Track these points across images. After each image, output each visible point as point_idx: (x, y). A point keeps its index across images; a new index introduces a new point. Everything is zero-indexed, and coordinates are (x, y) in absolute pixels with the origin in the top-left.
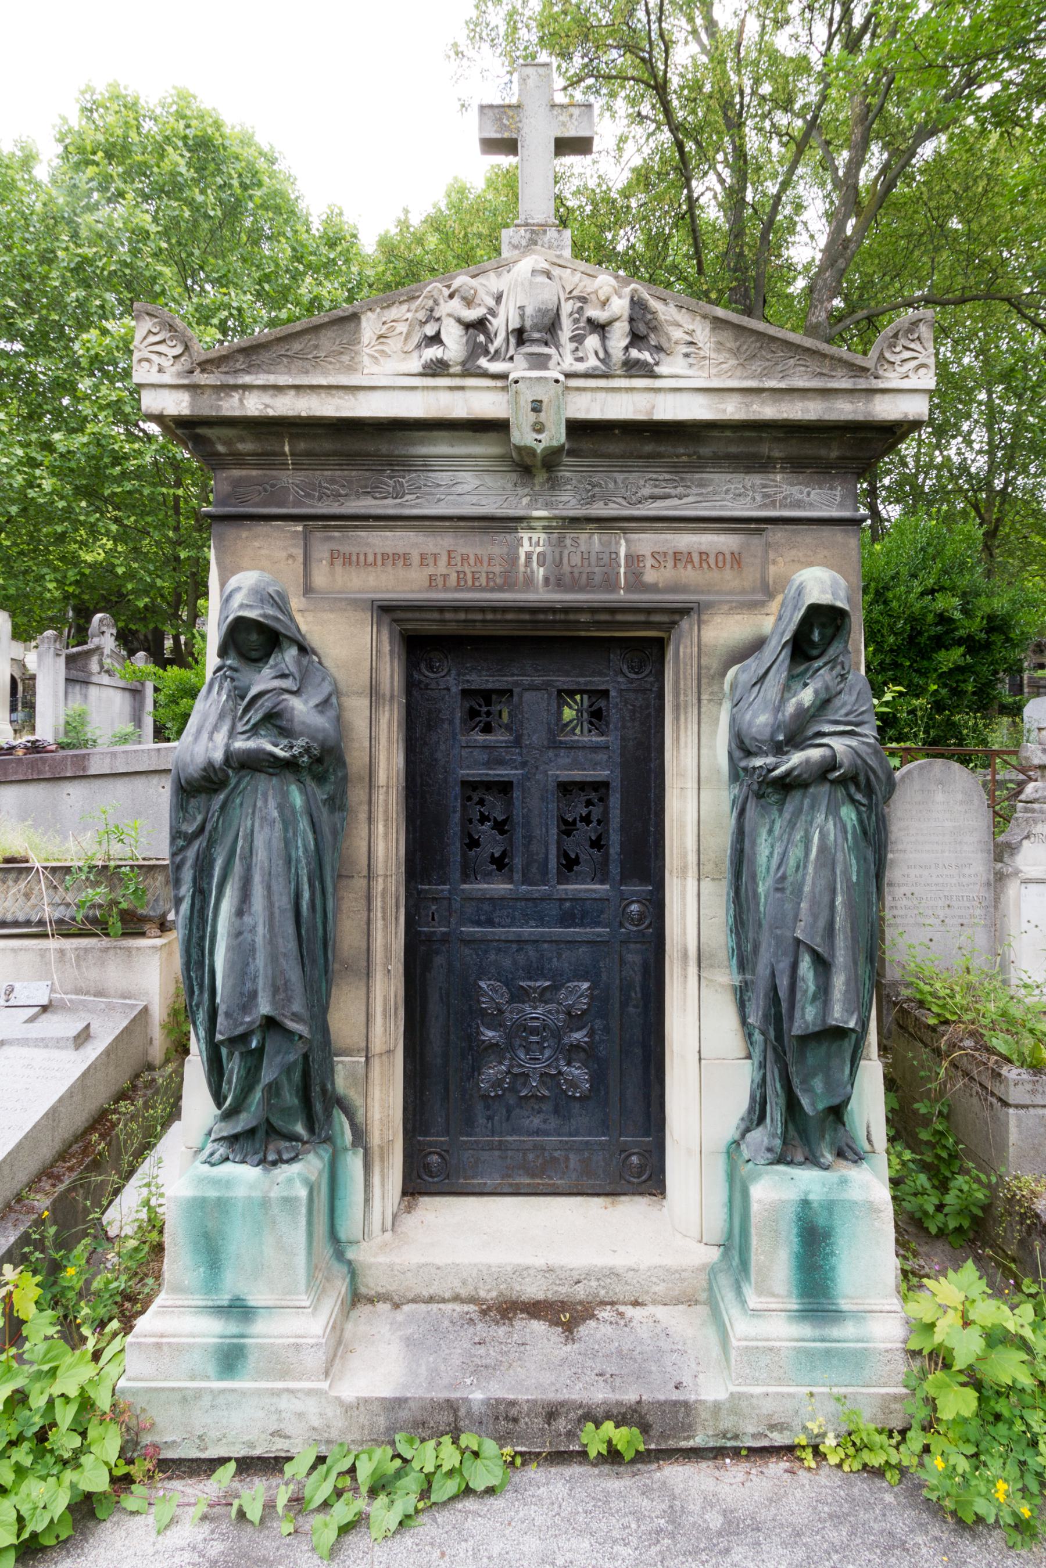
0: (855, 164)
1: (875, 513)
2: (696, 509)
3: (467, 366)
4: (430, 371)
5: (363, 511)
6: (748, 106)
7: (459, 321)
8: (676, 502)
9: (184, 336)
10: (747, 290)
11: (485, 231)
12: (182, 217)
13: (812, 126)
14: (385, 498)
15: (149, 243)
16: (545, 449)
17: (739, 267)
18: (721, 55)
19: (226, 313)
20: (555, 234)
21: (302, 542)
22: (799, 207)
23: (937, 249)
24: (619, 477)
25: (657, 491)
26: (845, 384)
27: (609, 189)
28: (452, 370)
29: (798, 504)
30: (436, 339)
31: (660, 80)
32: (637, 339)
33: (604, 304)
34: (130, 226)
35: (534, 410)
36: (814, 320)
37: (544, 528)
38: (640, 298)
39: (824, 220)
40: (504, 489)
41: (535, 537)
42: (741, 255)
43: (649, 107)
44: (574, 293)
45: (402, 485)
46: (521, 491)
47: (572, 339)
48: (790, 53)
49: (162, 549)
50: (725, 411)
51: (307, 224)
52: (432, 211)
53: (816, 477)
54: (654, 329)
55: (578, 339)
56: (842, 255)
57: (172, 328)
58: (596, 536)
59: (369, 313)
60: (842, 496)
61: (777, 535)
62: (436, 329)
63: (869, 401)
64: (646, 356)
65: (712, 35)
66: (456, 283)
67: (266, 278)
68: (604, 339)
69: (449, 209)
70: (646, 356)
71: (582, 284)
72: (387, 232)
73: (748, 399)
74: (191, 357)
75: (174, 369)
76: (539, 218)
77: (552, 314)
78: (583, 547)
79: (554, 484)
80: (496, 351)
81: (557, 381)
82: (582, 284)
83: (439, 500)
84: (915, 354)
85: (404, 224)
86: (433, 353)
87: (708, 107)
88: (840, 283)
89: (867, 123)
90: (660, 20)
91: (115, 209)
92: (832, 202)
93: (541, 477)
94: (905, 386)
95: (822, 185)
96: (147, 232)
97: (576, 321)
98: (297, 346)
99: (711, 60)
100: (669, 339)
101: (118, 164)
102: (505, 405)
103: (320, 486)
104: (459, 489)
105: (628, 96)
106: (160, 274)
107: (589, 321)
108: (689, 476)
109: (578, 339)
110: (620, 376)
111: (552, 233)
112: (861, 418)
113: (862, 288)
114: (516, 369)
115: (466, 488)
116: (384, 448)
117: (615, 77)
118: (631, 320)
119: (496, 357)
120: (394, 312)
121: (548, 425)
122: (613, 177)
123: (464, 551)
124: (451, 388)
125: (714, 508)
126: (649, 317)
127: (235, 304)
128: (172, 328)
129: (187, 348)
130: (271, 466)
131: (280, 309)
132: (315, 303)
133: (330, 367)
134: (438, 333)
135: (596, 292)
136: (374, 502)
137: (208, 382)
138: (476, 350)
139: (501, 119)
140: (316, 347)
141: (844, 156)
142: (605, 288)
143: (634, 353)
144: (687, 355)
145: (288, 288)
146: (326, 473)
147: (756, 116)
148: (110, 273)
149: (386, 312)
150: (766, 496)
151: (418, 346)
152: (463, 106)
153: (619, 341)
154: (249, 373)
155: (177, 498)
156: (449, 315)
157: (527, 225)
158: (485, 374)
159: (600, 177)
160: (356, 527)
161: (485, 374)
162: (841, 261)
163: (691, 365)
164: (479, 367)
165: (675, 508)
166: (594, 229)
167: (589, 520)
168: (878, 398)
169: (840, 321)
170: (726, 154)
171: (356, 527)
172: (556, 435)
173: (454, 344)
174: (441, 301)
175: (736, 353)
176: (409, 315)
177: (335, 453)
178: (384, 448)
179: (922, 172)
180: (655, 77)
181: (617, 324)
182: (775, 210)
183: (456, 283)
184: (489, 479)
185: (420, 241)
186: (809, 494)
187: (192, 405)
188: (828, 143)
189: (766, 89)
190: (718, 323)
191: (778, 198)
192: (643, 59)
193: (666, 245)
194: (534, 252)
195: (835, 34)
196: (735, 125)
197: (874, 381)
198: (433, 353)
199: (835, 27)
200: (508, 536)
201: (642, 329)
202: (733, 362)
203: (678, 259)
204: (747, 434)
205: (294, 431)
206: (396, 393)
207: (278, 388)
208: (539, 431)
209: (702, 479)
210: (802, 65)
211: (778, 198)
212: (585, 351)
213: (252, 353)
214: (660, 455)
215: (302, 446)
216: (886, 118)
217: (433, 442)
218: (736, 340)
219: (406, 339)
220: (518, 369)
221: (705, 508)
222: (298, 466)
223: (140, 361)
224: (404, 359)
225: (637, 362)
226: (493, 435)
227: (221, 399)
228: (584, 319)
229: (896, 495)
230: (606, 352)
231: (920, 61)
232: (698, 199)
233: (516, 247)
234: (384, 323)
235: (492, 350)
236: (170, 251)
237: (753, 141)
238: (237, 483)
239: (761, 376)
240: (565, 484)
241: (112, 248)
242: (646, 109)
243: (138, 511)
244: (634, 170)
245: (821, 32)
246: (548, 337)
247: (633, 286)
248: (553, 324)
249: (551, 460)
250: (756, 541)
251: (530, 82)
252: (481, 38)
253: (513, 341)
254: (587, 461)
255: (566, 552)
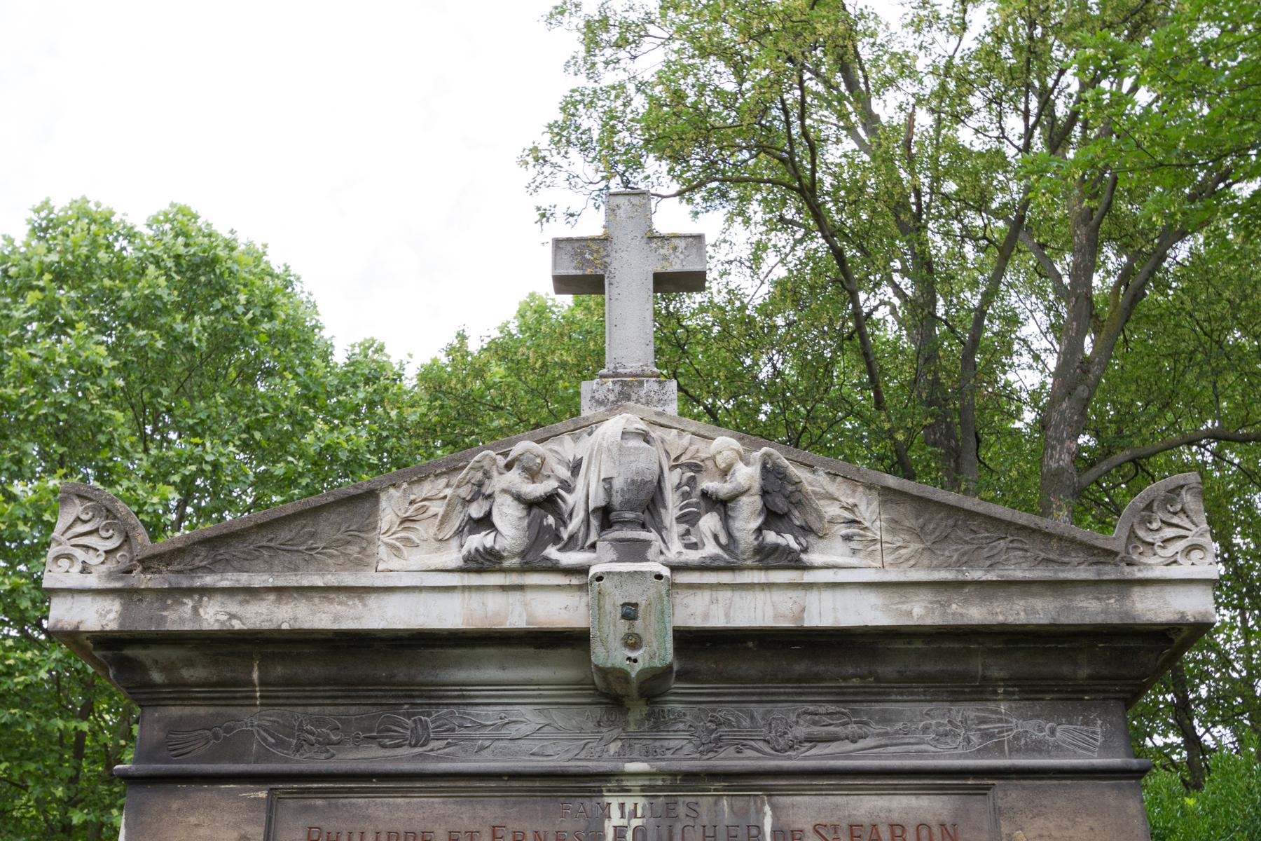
0: (1083, 272)
1: (1192, 741)
2: (878, 757)
3: (529, 558)
4: (473, 565)
5: (363, 767)
6: (928, 207)
7: (518, 498)
8: (850, 746)
9: (125, 522)
10: (949, 426)
11: (571, 359)
12: (152, 348)
13: (1017, 226)
14: (399, 746)
15: (99, 381)
16: (642, 672)
17: (935, 398)
18: (886, 152)
19: (193, 468)
20: (656, 387)
21: (264, 816)
22: (1013, 320)
23: (1217, 372)
24: (758, 710)
25: (817, 730)
26: (1085, 573)
27: (743, 307)
28: (506, 564)
29: (1037, 748)
30: (485, 523)
31: (806, 181)
32: (772, 518)
33: (725, 473)
34: (76, 361)
35: (625, 616)
36: (1053, 465)
37: (644, 789)
38: (774, 464)
39: (1051, 337)
40: (581, 730)
41: (629, 803)
42: (936, 382)
43: (794, 211)
44: (683, 460)
45: (425, 726)
46: (606, 733)
47: (680, 519)
48: (978, 147)
49: (45, 812)
50: (910, 613)
51: (325, 356)
52: (496, 334)
53: (1060, 705)
54: (798, 504)
55: (688, 519)
56: (1081, 381)
57: (110, 513)
58: (725, 802)
59: (392, 490)
60: (1104, 734)
61: (1010, 795)
62: (486, 508)
63: (1123, 597)
64: (789, 540)
65: (871, 132)
66: (517, 450)
67: (261, 425)
68: (726, 519)
69: (522, 332)
70: (789, 540)
71: (693, 448)
72: (435, 361)
73: (943, 597)
74: (131, 551)
75: (104, 568)
76: (633, 366)
77: (651, 487)
78: (705, 819)
79: (658, 721)
80: (571, 537)
81: (659, 577)
82: (693, 448)
83: (482, 748)
84: (1183, 532)
85: (458, 350)
86: (477, 541)
87: (874, 211)
88: (1083, 414)
89: (1092, 223)
90: (802, 118)
91: (59, 341)
92: (1058, 315)
93: (638, 711)
94: (1178, 576)
95: (1042, 294)
96: (100, 369)
97: (685, 495)
98: (285, 534)
99: (874, 158)
100: (821, 518)
101: (73, 288)
102: (583, 610)
103: (301, 730)
104: (513, 731)
105: (764, 200)
106: (109, 419)
107: (705, 494)
108: (864, 707)
109: (688, 519)
110: (752, 568)
111: (650, 385)
112: (1115, 620)
113: (1119, 421)
114: (599, 561)
115: (524, 729)
116: (401, 673)
117: (746, 180)
118: (764, 493)
119: (570, 544)
120: (427, 489)
121: (648, 637)
122: (750, 292)
123: (517, 827)
124: (504, 588)
125: (906, 755)
126: (790, 488)
127: (209, 458)
128: (110, 513)
129: (127, 539)
130: (230, 701)
131: (274, 463)
132: (327, 454)
133: (330, 561)
134: (488, 516)
135: (713, 458)
136: (381, 753)
137: (150, 585)
138: (540, 537)
139: (582, 254)
140: (312, 535)
141: (1064, 265)
142: (725, 453)
143: (771, 537)
144: (847, 538)
145: (290, 436)
146: (311, 710)
147: (940, 216)
148: (38, 418)
149: (416, 488)
150: (986, 735)
151: (459, 532)
152: (543, 215)
153: (748, 520)
154: (211, 571)
155: (81, 735)
156: (505, 491)
157: (616, 375)
158: (555, 568)
159: (729, 292)
160: (351, 790)
161: (555, 568)
162: (1081, 388)
163: (854, 551)
164: (547, 559)
165: (846, 755)
166: (723, 353)
167: (713, 775)
168: (1137, 593)
169: (1092, 465)
170: (903, 262)
171: (351, 790)
172: (658, 651)
173: (510, 527)
174: (495, 474)
175: (918, 534)
176: (448, 492)
177: (326, 682)
178: (401, 673)
179: (1177, 279)
180: (799, 179)
181: (744, 499)
182: (978, 327)
183: (517, 450)
184: (558, 717)
185: (479, 373)
186: (1053, 732)
187: (123, 616)
188: (1043, 246)
189: (950, 187)
190: (889, 496)
191: (981, 312)
192: (782, 160)
193: (828, 372)
194: (626, 409)
195: (1034, 127)
196: (914, 228)
197: (1127, 569)
198: (477, 541)
199: (1032, 120)
200: (587, 802)
201: (780, 504)
202: (915, 546)
203: (845, 390)
204: (947, 645)
205: (269, 650)
206: (423, 596)
207: (251, 593)
208: (634, 646)
209: (884, 711)
210: (995, 160)
211: (981, 312)
212: (700, 534)
213: (219, 546)
214: (818, 678)
215: (279, 671)
216: (1116, 217)
217: (477, 663)
218: (917, 517)
219: (442, 523)
220: (603, 561)
221: (894, 756)
222: (269, 701)
223: (57, 558)
224: (438, 549)
225: (776, 547)
226: (566, 652)
227: (166, 608)
228: (697, 492)
229: (1220, 711)
230: (730, 535)
231: (1147, 160)
232: (869, 314)
233: (600, 403)
234: (412, 503)
235: (565, 536)
236: (127, 391)
237: (937, 244)
238: (174, 727)
239: (959, 565)
240: (676, 721)
241: (45, 386)
242: (790, 214)
243: (17, 754)
244: (779, 283)
245: (1015, 125)
246: (645, 517)
247: (764, 449)
248: (653, 500)
249: (653, 688)
250: (977, 805)
251: (621, 213)
252: (569, 142)
253: (594, 523)
254: (707, 687)
255: (678, 827)
